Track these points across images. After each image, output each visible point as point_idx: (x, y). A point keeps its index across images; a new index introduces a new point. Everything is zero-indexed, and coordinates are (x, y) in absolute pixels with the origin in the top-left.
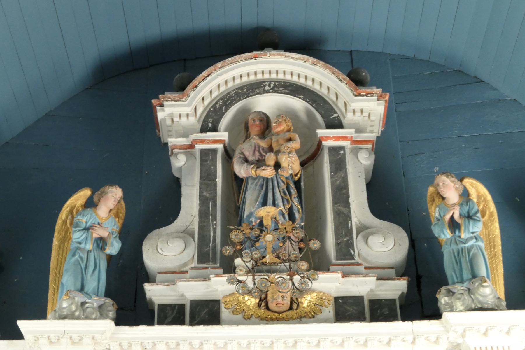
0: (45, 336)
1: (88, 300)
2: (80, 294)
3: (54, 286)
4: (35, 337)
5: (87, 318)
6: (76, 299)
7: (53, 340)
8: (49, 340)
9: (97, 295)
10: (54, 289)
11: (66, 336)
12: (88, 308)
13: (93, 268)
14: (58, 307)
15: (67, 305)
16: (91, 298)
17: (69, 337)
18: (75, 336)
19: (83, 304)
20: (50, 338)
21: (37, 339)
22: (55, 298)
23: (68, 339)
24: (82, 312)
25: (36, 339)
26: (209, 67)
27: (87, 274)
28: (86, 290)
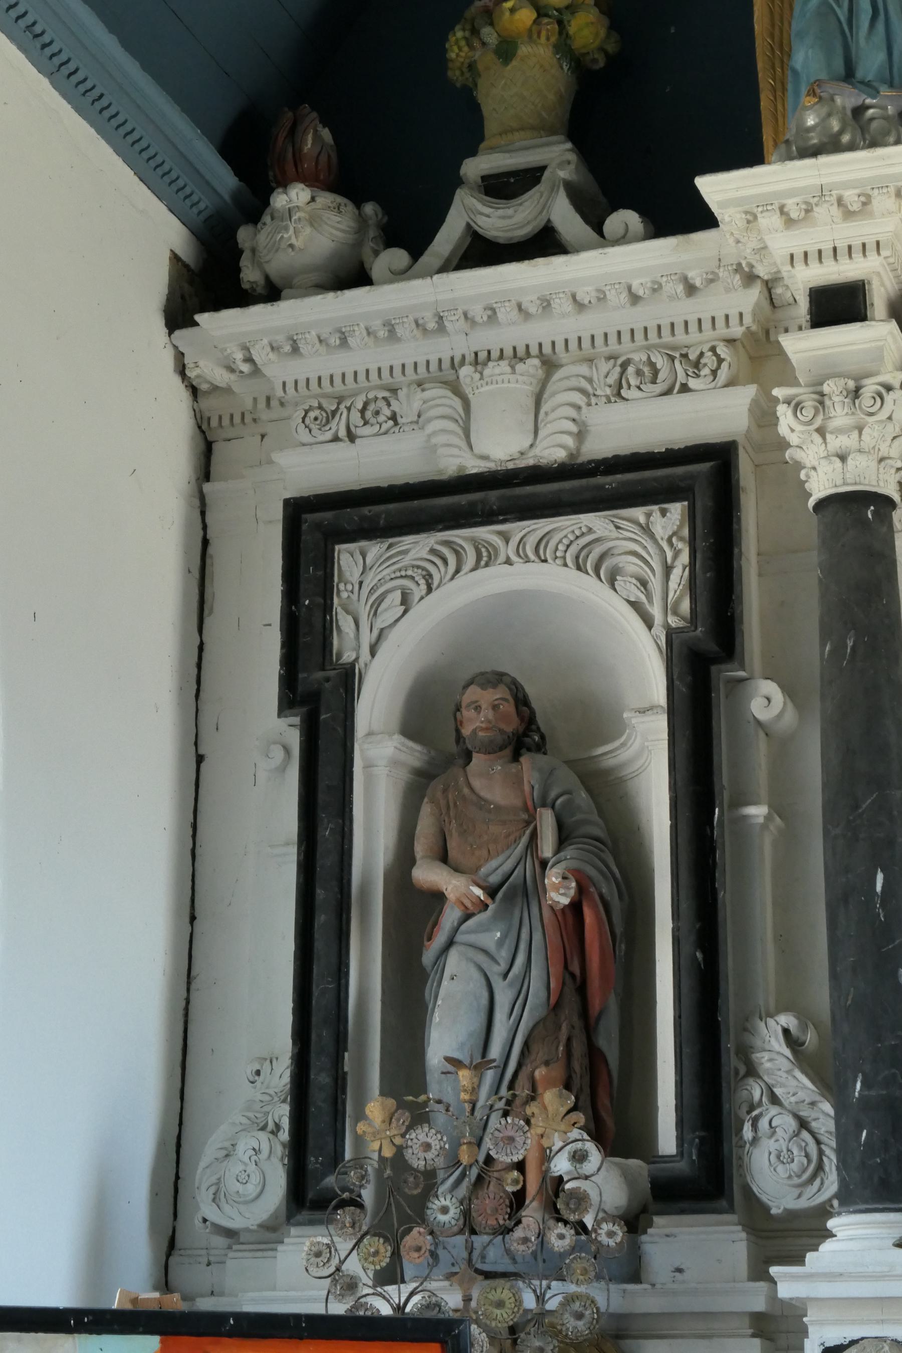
0: (773, 207)
1: (869, 101)
2: (847, 88)
3: (773, 83)
4: (746, 213)
5: (873, 144)
6: (839, 100)
7: (794, 215)
8: (784, 217)
9: (891, 85)
10: (774, 90)
11: (827, 199)
12: (872, 119)
13: (870, 16)
14: (794, 131)
15: (817, 120)
16: (878, 92)
17: (834, 199)
18: (850, 196)
19: (858, 111)
20: (786, 210)
21: (752, 219)
22: (779, 113)
23: (832, 205)
24: (859, 132)
25: (749, 217)
26: (440, 228)
27: (857, 33)
28: (859, 74)
